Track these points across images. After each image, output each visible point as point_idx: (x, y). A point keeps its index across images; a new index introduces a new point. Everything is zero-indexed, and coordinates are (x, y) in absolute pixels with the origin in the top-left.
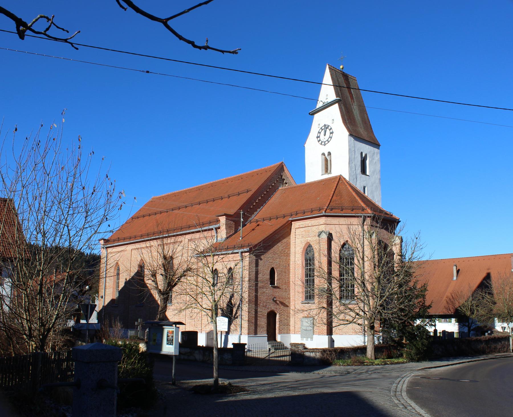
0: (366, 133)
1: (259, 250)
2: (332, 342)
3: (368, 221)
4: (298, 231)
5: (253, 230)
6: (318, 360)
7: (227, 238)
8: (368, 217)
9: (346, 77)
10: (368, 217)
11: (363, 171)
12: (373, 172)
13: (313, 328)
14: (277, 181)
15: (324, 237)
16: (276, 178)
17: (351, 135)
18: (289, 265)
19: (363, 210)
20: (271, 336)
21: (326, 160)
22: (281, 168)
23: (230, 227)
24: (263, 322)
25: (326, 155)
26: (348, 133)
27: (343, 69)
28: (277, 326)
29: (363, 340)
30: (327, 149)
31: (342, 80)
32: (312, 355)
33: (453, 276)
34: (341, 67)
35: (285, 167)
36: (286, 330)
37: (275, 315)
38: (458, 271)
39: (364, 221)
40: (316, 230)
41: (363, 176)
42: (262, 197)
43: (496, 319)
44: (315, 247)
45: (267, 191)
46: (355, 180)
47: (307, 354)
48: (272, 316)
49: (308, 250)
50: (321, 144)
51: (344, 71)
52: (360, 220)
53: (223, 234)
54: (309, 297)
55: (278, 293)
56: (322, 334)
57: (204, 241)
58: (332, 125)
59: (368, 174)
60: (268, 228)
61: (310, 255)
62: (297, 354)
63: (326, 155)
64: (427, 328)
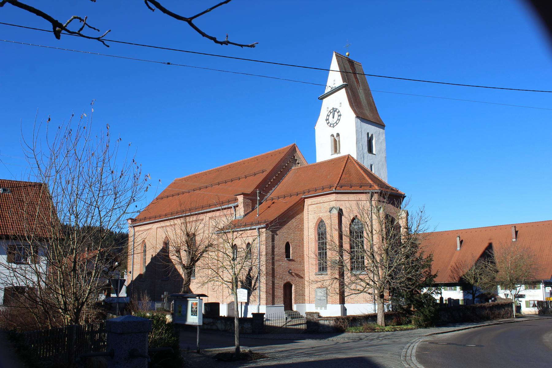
0: (372, 115)
1: (275, 226)
3: (376, 196)
4: (310, 207)
6: (332, 327)
7: (245, 215)
8: (376, 193)
9: (351, 62)
10: (376, 193)
11: (370, 150)
12: (379, 151)
14: (290, 161)
15: (335, 212)
16: (290, 158)
17: (357, 117)
18: (303, 239)
19: (371, 186)
20: (288, 306)
21: (335, 141)
22: (293, 150)
23: (247, 205)
24: (280, 293)
25: (335, 136)
26: (355, 116)
29: (373, 309)
30: (336, 130)
31: (348, 66)
32: (326, 323)
33: (457, 247)
34: (347, 54)
35: (297, 149)
36: (302, 300)
37: (291, 286)
39: (372, 196)
40: (327, 206)
41: (370, 155)
42: (276, 177)
43: (499, 286)
44: (327, 222)
45: (281, 171)
47: (322, 322)
48: (288, 287)
50: (330, 126)
53: (241, 211)
54: (322, 269)
55: (293, 265)
56: (335, 303)
57: (223, 219)
58: (339, 109)
59: (374, 152)
61: (322, 229)
62: (312, 322)
64: (434, 296)
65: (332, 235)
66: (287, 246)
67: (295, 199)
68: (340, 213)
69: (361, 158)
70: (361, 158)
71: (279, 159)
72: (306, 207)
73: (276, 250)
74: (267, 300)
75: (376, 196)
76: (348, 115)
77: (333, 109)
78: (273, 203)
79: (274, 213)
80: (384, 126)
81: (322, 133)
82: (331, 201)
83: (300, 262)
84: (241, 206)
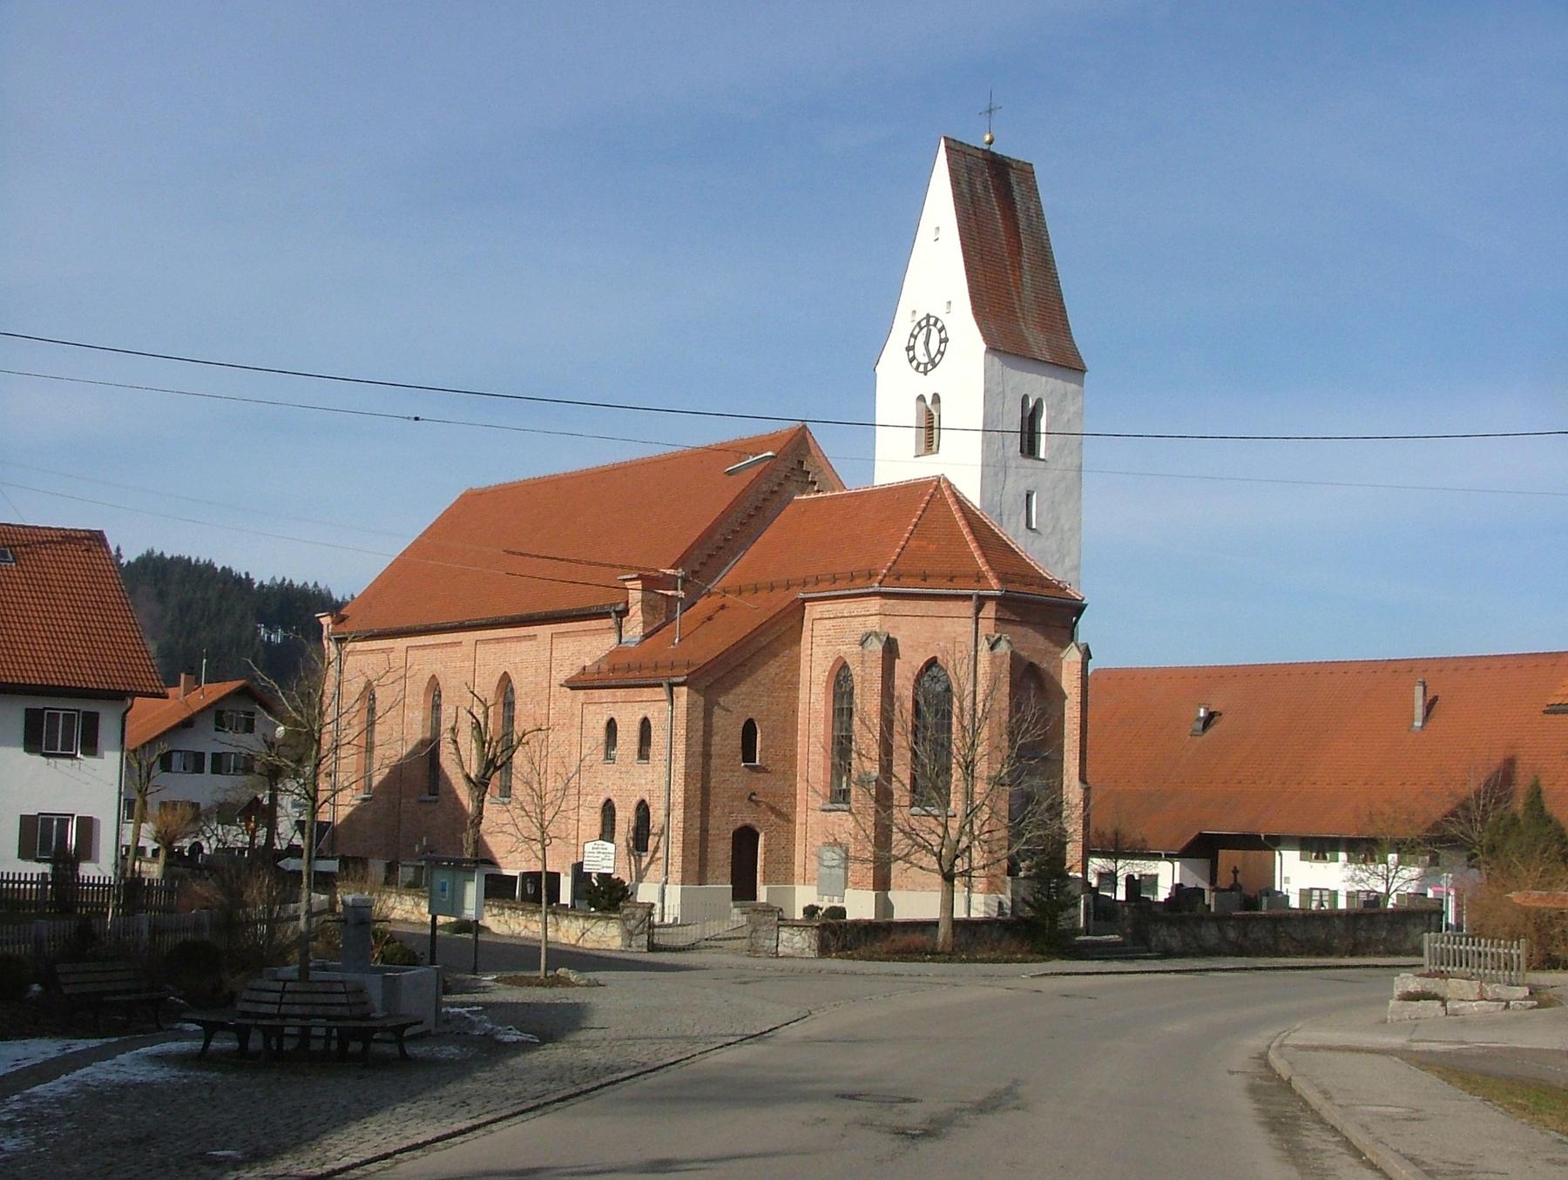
1: (712, 680)
2: (884, 906)
3: (990, 610)
4: (818, 626)
5: (710, 619)
7: (646, 636)
11: (1029, 447)
13: (846, 868)
15: (876, 647)
16: (794, 460)
17: (992, 349)
18: (795, 712)
19: (979, 577)
21: (930, 415)
23: (653, 608)
24: (722, 851)
25: (929, 401)
26: (984, 346)
27: (990, 142)
28: (760, 863)
36: (784, 872)
37: (755, 836)
38: (1429, 707)
39: (978, 610)
40: (860, 627)
41: (1028, 462)
43: (46, 868)
44: (856, 670)
46: (1001, 475)
48: (745, 841)
49: (841, 681)
51: (993, 148)
52: (967, 608)
53: (634, 627)
54: (840, 796)
55: (760, 783)
57: (588, 646)
58: (945, 320)
59: (1042, 456)
60: (750, 612)
61: (845, 688)
63: (929, 401)
65: (867, 701)
66: (749, 730)
67: (781, 599)
68: (891, 649)
69: (996, 474)
70: (996, 474)
71: (729, 497)
72: (807, 624)
73: (716, 739)
74: (684, 870)
75: (990, 610)
76: (967, 341)
77: (928, 317)
78: (723, 607)
79: (716, 641)
80: (1083, 371)
81: (896, 388)
82: (867, 615)
83: (785, 773)
84: (636, 610)
